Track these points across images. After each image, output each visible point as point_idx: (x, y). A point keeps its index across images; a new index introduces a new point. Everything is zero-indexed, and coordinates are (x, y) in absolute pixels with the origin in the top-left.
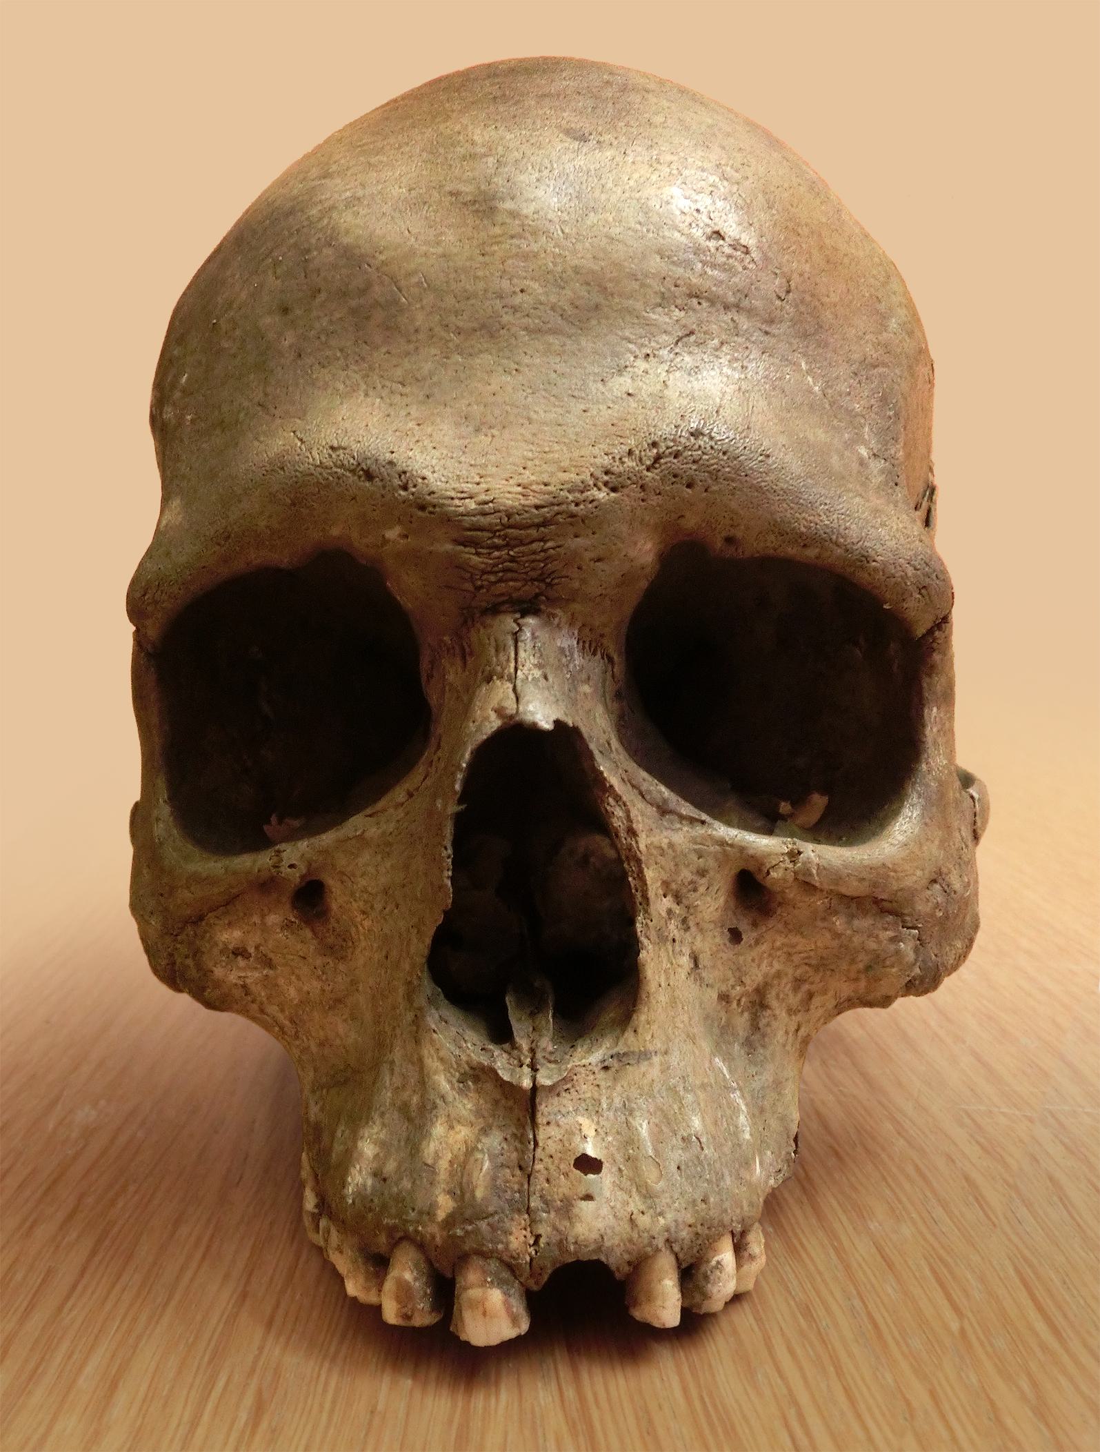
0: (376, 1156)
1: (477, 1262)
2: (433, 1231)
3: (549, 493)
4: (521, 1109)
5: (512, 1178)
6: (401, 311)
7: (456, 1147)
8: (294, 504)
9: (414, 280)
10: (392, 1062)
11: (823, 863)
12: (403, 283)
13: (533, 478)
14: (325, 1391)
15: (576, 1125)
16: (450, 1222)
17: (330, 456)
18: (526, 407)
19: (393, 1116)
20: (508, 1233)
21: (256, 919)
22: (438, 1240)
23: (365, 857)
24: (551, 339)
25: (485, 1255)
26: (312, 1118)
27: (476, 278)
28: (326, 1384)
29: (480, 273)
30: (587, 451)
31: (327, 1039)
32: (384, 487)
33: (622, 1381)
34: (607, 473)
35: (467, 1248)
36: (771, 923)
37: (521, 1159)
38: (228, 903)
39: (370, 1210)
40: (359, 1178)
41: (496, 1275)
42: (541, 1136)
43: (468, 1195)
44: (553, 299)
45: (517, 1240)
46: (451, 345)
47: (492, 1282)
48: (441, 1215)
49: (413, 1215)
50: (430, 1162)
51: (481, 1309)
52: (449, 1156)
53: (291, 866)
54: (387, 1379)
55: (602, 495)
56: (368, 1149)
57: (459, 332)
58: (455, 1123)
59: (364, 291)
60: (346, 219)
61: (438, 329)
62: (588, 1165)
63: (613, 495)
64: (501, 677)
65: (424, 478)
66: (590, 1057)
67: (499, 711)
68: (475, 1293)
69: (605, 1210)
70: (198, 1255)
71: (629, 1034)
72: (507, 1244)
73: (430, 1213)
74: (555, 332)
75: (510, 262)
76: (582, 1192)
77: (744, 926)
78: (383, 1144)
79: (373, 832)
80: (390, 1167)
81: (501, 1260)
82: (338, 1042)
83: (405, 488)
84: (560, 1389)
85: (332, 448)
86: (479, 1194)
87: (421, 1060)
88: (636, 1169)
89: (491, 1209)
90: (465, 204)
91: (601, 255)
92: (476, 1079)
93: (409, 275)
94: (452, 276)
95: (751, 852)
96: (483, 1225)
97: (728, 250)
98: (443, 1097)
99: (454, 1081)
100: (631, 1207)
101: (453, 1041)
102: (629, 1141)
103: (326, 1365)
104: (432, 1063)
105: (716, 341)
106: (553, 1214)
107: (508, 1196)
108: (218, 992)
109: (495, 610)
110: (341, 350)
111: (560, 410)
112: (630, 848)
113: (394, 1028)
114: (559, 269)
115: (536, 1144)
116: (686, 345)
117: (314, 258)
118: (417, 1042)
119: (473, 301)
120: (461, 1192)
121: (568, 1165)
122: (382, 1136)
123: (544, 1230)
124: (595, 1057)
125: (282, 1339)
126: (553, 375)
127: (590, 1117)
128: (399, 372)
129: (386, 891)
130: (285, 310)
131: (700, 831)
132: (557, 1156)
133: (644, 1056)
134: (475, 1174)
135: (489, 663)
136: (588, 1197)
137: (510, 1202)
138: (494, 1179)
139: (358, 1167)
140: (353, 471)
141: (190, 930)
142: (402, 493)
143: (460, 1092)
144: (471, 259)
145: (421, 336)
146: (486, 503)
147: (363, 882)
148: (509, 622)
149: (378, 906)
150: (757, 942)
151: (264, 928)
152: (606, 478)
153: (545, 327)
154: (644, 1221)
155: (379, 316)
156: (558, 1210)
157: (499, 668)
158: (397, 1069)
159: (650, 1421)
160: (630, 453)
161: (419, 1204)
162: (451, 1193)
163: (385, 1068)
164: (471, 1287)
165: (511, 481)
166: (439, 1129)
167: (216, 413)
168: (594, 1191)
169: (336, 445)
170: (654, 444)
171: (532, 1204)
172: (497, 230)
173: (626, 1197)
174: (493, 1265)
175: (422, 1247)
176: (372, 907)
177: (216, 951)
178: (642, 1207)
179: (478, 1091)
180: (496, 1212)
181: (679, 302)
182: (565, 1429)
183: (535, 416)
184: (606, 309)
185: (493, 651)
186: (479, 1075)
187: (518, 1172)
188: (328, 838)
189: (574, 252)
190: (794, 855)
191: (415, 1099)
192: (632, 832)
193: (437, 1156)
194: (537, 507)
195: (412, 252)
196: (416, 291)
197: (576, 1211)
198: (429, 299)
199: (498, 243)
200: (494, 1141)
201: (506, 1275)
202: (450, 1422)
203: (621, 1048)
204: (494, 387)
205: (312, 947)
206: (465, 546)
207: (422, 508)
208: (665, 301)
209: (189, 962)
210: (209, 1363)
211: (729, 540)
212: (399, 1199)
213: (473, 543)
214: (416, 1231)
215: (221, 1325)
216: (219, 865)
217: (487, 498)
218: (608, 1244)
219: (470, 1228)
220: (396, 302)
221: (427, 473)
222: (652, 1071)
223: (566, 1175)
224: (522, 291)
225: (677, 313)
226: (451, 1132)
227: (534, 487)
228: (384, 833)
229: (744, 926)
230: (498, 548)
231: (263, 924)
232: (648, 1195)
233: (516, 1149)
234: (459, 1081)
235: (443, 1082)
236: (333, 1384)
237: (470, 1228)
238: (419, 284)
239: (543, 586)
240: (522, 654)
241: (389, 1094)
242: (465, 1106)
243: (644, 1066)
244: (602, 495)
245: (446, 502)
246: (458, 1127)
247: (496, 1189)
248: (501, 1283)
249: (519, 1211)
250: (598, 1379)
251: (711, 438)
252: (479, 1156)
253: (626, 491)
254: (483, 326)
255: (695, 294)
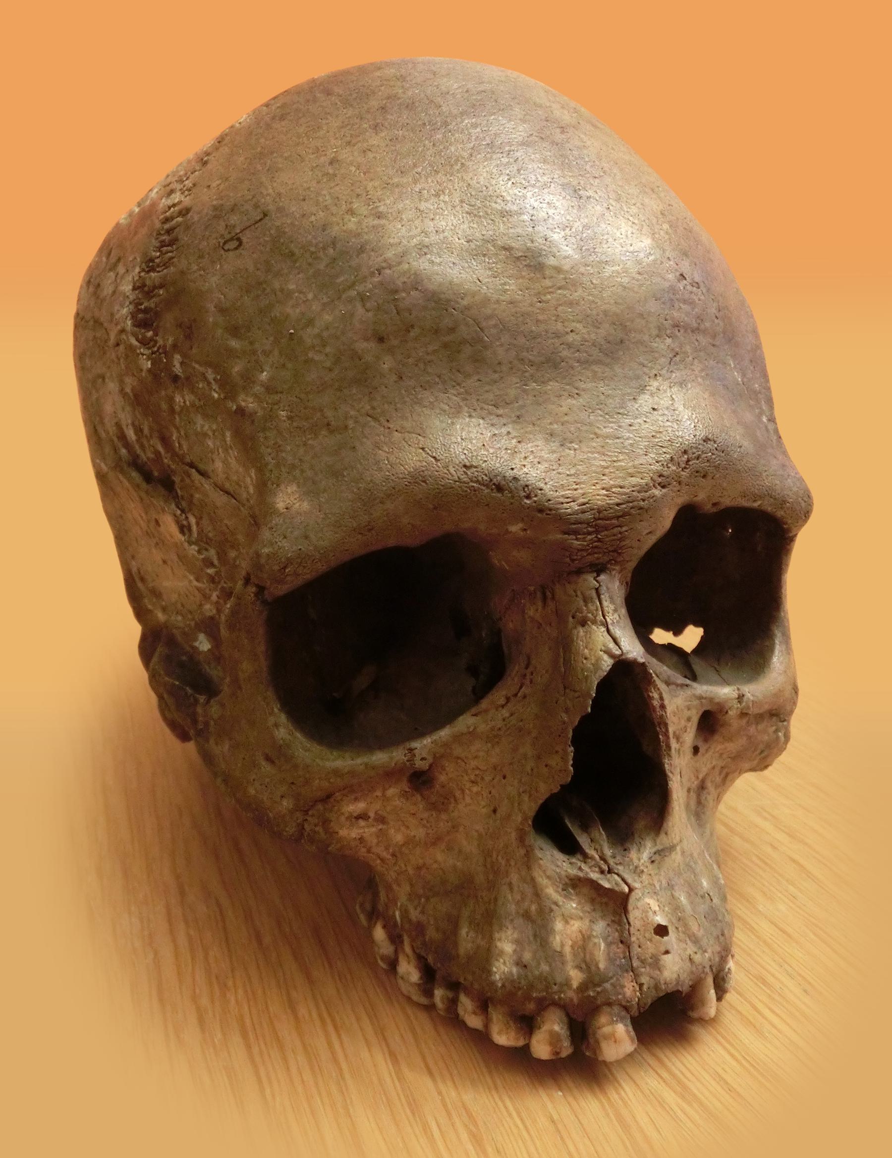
0: (515, 951)
1: (606, 1009)
2: (571, 995)
3: (626, 494)
4: (615, 904)
5: (620, 949)
6: (485, 347)
7: (574, 935)
8: (435, 508)
9: (493, 322)
10: (510, 884)
11: (755, 699)
12: (484, 324)
13: (612, 482)
14: (510, 1115)
15: (648, 907)
16: (583, 987)
17: (466, 473)
18: (591, 424)
19: (519, 921)
20: (623, 987)
21: (379, 793)
22: (576, 1001)
23: (477, 746)
24: (595, 368)
25: (609, 1004)
26: (414, 919)
27: (538, 321)
28: (506, 1108)
29: (540, 317)
30: (643, 460)
31: (424, 864)
32: (513, 497)
33: (690, 1058)
34: (660, 476)
35: (599, 1002)
36: (716, 737)
37: (621, 935)
38: (354, 787)
39: (519, 989)
40: (503, 968)
41: (618, 1015)
42: (631, 919)
43: (593, 968)
44: (593, 336)
45: (629, 989)
46: (527, 374)
47: (617, 1021)
48: (575, 984)
49: (556, 988)
50: (558, 949)
51: (613, 1039)
52: (570, 943)
53: (423, 759)
54: (543, 1094)
55: (657, 492)
56: (507, 947)
57: (532, 364)
58: (569, 920)
59: (452, 330)
60: (422, 265)
61: (516, 362)
62: (661, 931)
63: (663, 490)
64: (594, 622)
65: (541, 490)
66: (642, 854)
67: (608, 652)
68: (607, 1030)
69: (677, 959)
70: (330, 1028)
71: (662, 836)
72: (624, 994)
73: (567, 983)
74: (599, 362)
75: (560, 308)
76: (663, 949)
77: (700, 744)
78: (517, 942)
79: (483, 728)
80: (527, 956)
81: (621, 1005)
82: (435, 866)
83: (528, 497)
84: (657, 1072)
85: (465, 466)
86: (602, 966)
87: (533, 879)
88: (686, 925)
89: (611, 974)
90: (518, 258)
91: (620, 301)
92: (574, 887)
93: (488, 318)
94: (520, 319)
95: (717, 700)
96: (607, 986)
97: (689, 287)
98: (556, 904)
99: (560, 890)
100: (689, 952)
101: (552, 863)
102: (676, 908)
103: (494, 1092)
104: (543, 881)
105: (690, 358)
106: (648, 967)
107: (618, 962)
108: (339, 845)
109: (579, 572)
110: (439, 377)
111: (615, 426)
112: (661, 717)
113: (508, 860)
114: (594, 312)
115: (629, 923)
116: (676, 364)
117: (404, 299)
118: (529, 868)
119: (539, 340)
120: (586, 964)
121: (650, 934)
122: (515, 936)
123: (644, 980)
124: (645, 855)
125: (450, 1083)
126: (602, 397)
127: (652, 897)
128: (491, 396)
129: (495, 768)
130: (381, 340)
131: (689, 692)
132: (642, 929)
133: (672, 848)
134: (596, 953)
135: (579, 610)
136: (667, 952)
137: (620, 966)
138: (608, 954)
139: (502, 961)
140: (487, 486)
141: (320, 807)
142: (528, 502)
143: (566, 897)
144: (531, 305)
145: (504, 368)
146: (584, 504)
147: (474, 763)
148: (590, 580)
149: (488, 778)
150: (707, 751)
151: (385, 799)
152: (660, 480)
153: (591, 359)
154: (697, 958)
155: (467, 350)
156: (650, 965)
157: (590, 615)
158: (516, 889)
159: (724, 1080)
160: (672, 459)
161: (559, 979)
162: (579, 967)
163: (505, 888)
164: (604, 1026)
165: (598, 487)
166: (559, 925)
167: (319, 414)
168: (669, 948)
169: (468, 464)
170: (685, 452)
171: (635, 965)
172: (548, 283)
173: (684, 945)
174: (616, 1009)
175: (563, 1006)
176: (482, 779)
177: (343, 819)
178: (695, 950)
179: (577, 894)
180: (614, 975)
181: (668, 332)
182: (680, 1101)
183: (599, 432)
184: (627, 342)
185: (582, 603)
186: (576, 884)
187: (621, 945)
188: (444, 733)
189: (602, 298)
190: (740, 697)
191: (533, 908)
192: (663, 707)
193: (562, 945)
194: (618, 505)
195: (486, 300)
196: (494, 331)
197: (662, 962)
198: (505, 338)
199: (550, 293)
200: (600, 927)
201: (624, 1013)
202: (608, 1115)
203: (659, 847)
204: (565, 409)
205: (421, 806)
206: (569, 534)
207: (541, 511)
208: (661, 332)
209: (319, 829)
210: (413, 1114)
211: (714, 504)
212: (543, 978)
213: (576, 532)
214: (560, 998)
215: (396, 1081)
216: (359, 761)
217: (585, 500)
218: (682, 978)
219: (599, 989)
220: (481, 340)
221: (542, 485)
222: (676, 857)
223: (651, 940)
224: (572, 331)
225: (669, 341)
226: (568, 926)
227: (614, 490)
228: (492, 729)
229: (700, 744)
230: (589, 533)
231: (384, 795)
232: (696, 941)
233: (617, 930)
234: (563, 890)
235: (551, 892)
236: (511, 1108)
237: (599, 989)
238: (495, 326)
239: (616, 555)
240: (605, 604)
241: (513, 906)
242: (572, 905)
243: (673, 855)
244: (657, 492)
245: (559, 506)
246: (572, 922)
247: (611, 960)
248: (622, 1019)
249: (627, 971)
250: (674, 1059)
251: (715, 442)
252: (596, 940)
253: (670, 486)
254: (548, 360)
255: (676, 326)
